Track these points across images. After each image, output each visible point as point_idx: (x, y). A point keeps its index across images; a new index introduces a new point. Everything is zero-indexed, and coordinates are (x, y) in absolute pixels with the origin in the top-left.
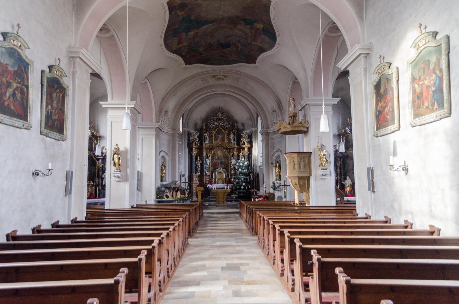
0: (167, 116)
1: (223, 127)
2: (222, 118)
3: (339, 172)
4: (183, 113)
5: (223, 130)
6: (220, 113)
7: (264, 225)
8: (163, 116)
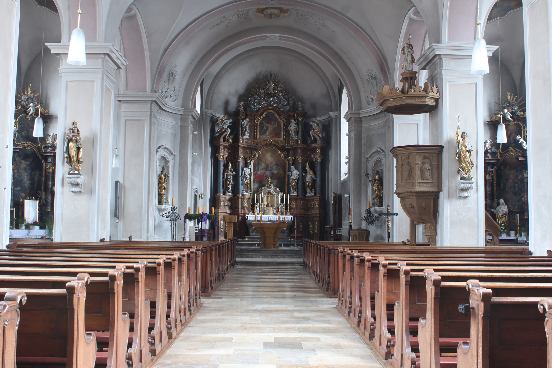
0: (173, 81)
1: (275, 109)
2: (276, 93)
3: (489, 191)
4: (202, 79)
5: (276, 116)
6: (271, 83)
7: (352, 270)
8: (165, 82)
